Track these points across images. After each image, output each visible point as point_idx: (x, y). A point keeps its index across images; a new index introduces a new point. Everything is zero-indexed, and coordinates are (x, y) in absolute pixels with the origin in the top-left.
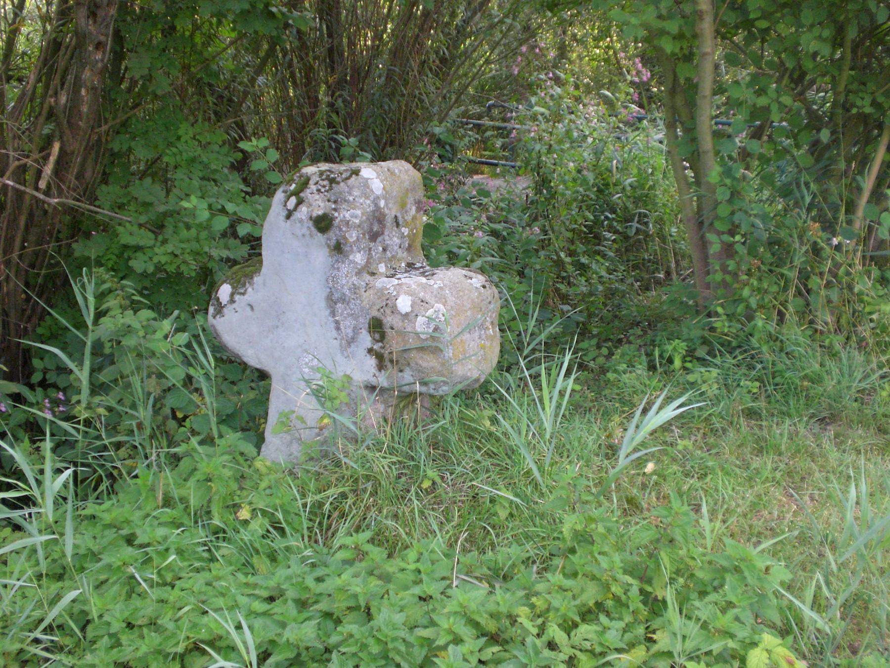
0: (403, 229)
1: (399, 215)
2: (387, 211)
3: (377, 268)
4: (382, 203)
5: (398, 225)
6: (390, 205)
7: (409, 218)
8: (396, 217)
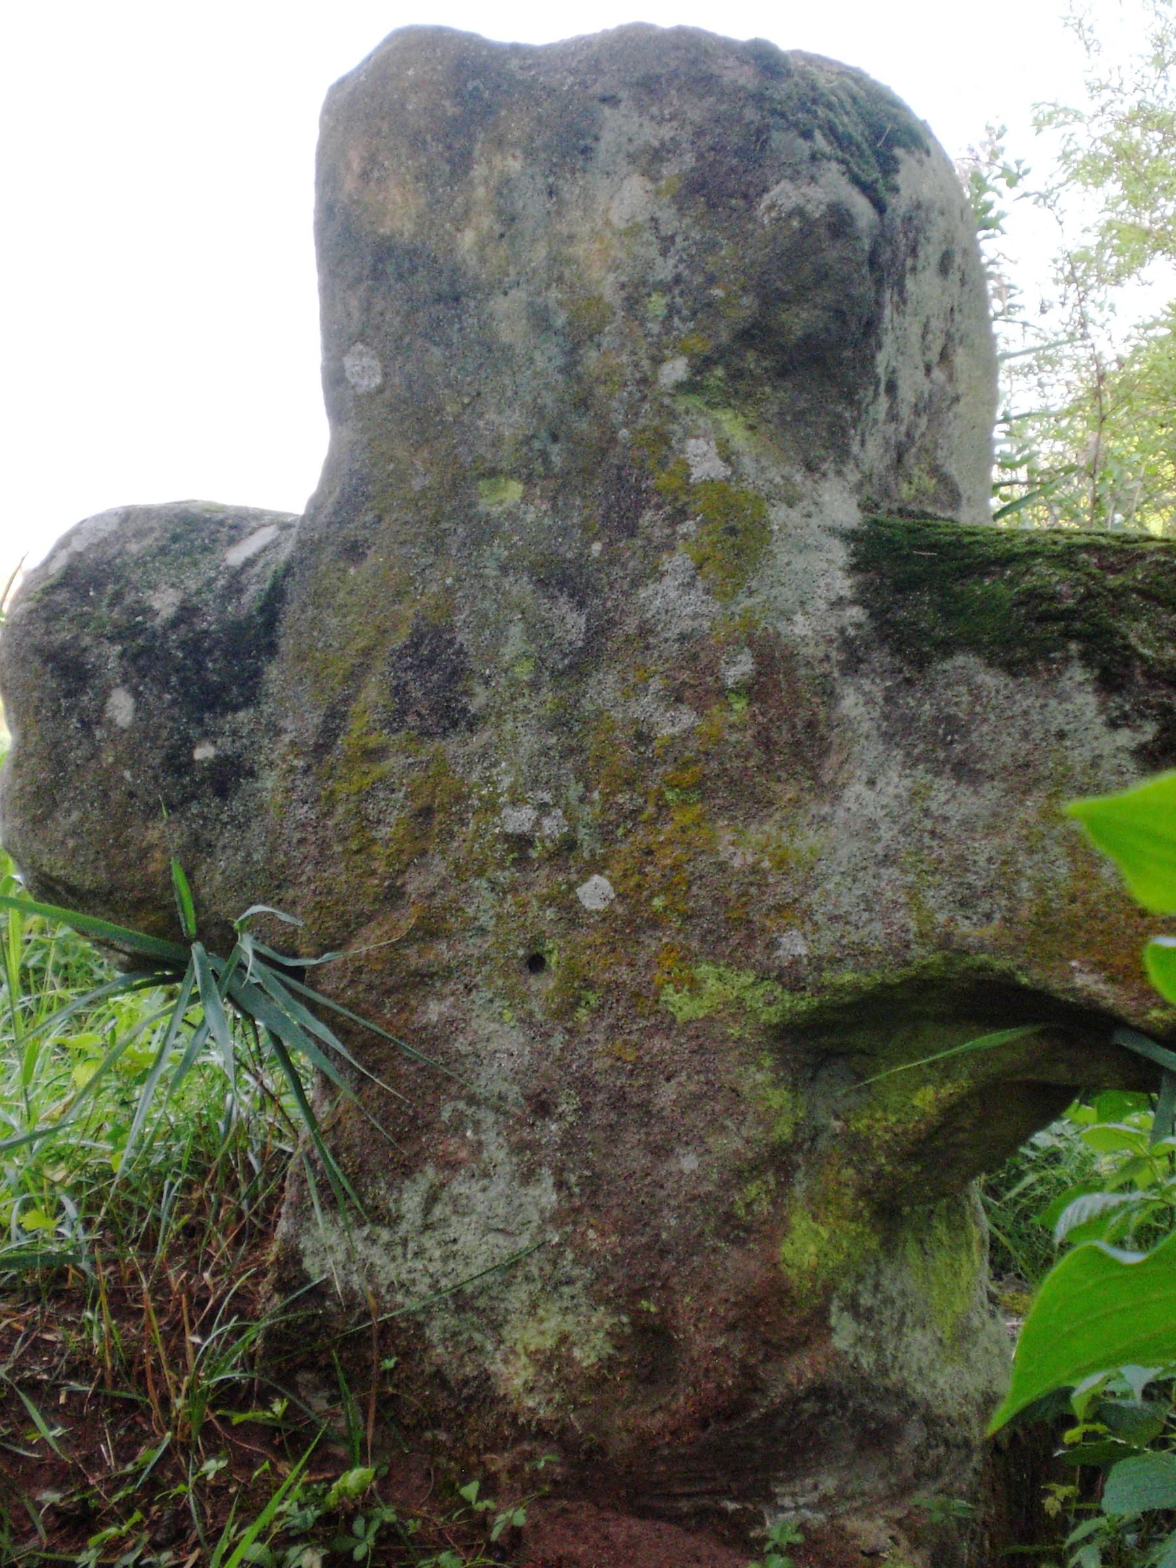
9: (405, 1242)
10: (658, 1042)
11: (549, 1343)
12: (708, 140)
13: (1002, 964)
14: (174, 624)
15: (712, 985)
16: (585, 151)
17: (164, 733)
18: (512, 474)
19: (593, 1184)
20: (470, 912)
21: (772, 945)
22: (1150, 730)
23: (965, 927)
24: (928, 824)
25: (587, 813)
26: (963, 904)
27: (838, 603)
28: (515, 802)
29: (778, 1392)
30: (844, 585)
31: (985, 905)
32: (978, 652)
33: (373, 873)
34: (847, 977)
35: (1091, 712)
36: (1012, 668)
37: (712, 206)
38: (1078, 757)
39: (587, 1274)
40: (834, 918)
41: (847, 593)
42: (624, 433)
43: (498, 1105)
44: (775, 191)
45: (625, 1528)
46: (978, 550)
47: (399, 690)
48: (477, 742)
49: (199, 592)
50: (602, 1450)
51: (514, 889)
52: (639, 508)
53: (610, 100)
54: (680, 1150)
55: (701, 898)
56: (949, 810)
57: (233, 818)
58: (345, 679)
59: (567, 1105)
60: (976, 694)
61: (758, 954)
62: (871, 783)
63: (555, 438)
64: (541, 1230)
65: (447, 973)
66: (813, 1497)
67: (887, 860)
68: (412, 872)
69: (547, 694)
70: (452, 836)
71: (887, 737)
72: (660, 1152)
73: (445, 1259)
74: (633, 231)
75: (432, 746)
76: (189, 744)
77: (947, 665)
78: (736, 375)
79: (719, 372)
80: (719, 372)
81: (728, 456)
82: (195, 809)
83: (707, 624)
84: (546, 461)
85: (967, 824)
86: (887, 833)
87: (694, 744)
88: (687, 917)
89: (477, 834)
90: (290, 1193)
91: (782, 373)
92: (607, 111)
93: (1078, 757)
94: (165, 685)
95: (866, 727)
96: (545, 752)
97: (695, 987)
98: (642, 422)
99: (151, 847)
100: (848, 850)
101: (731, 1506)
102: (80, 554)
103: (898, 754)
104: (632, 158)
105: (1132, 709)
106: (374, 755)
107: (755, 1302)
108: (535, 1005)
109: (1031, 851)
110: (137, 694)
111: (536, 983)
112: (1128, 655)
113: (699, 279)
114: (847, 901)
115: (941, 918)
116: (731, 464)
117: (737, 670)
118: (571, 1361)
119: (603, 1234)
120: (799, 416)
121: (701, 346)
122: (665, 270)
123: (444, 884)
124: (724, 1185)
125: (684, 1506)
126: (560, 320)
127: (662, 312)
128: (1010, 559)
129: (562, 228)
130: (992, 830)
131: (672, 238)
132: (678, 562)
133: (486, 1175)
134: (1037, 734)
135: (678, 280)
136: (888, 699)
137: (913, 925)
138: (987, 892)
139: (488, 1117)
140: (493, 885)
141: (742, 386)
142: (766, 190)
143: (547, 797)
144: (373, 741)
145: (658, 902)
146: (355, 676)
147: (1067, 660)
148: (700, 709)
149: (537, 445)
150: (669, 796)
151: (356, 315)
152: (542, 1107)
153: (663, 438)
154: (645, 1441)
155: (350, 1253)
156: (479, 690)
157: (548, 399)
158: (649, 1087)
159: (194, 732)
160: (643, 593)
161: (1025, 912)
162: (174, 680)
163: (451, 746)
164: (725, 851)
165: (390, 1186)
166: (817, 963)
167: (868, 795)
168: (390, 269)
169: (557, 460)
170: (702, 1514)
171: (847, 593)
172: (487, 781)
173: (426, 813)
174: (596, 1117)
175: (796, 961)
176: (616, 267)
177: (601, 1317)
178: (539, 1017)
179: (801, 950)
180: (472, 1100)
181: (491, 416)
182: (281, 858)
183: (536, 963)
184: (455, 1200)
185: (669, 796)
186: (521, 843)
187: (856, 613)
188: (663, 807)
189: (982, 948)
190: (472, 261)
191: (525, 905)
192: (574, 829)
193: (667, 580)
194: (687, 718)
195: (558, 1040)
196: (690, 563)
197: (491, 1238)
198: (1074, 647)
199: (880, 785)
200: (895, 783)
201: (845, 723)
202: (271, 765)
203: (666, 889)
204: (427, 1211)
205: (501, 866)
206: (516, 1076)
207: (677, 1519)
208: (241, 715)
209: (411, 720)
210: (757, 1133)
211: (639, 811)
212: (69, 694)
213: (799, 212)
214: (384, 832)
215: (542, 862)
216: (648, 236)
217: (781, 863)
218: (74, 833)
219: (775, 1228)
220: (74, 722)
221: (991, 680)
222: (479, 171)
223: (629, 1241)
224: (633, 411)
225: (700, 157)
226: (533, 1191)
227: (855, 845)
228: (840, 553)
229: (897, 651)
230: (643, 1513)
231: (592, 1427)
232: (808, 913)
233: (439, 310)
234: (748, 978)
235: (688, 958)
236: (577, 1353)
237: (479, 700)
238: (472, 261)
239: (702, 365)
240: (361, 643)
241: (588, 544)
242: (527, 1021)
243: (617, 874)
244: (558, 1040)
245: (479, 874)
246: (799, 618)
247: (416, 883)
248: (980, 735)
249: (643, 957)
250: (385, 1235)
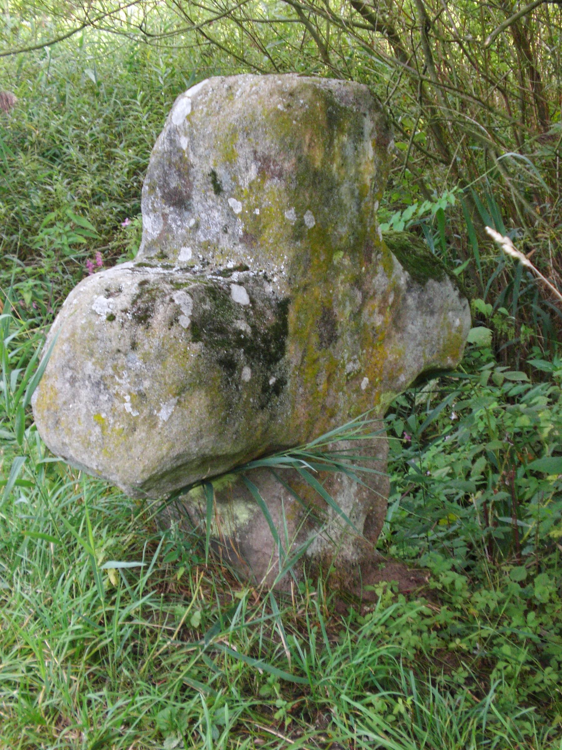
0: (232, 202)
1: (220, 172)
2: (192, 159)
3: (176, 252)
4: (184, 142)
5: (218, 190)
6: (201, 150)
7: (244, 184)
8: (214, 174)
13: (434, 364)
76: (267, 379)
90: (158, 653)
94: (259, 360)
103: (419, 313)
105: (76, 305)
110: (251, 367)
116: (165, 181)
129: (358, 161)
167: (413, 327)
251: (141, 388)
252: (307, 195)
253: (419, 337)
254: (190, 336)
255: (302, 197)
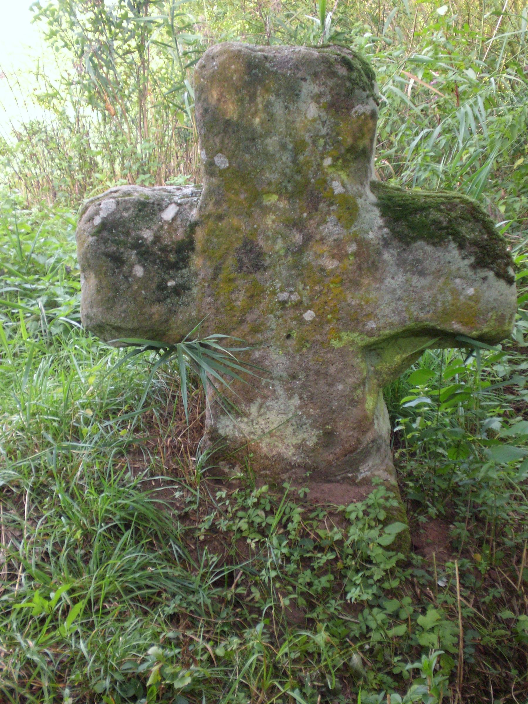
9: (252, 421)
10: (329, 355)
11: (300, 441)
12: (335, 92)
13: (432, 324)
14: (154, 243)
15: (345, 337)
16: (297, 95)
17: (156, 278)
18: (274, 193)
19: (311, 397)
20: (268, 324)
21: (364, 325)
22: (472, 259)
23: (422, 315)
24: (411, 289)
25: (305, 293)
26: (421, 309)
27: (380, 228)
28: (282, 291)
29: (365, 444)
30: (380, 222)
31: (428, 309)
32: (424, 240)
33: (235, 316)
34: (387, 332)
35: (457, 256)
36: (434, 244)
37: (337, 111)
38: (453, 268)
39: (310, 421)
40: (383, 316)
41: (382, 224)
42: (313, 180)
43: (280, 378)
44: (357, 107)
45: (326, 486)
46: (412, 206)
47: (240, 261)
48: (267, 274)
49: (159, 231)
50: (317, 468)
51: (282, 316)
52: (318, 203)
53: (304, 80)
54: (337, 384)
55: (342, 314)
56: (418, 284)
57: (183, 303)
58: (220, 258)
59: (302, 376)
60: (425, 253)
61: (360, 327)
62: (393, 278)
63: (289, 182)
64: (296, 411)
65: (261, 343)
66: (367, 469)
67: (399, 299)
68: (247, 315)
69: (290, 258)
70: (260, 302)
71: (398, 265)
72: (331, 385)
73: (266, 424)
74: (314, 120)
75: (252, 276)
76: (165, 281)
77: (415, 245)
78: (344, 161)
79: (340, 161)
80: (340, 161)
81: (344, 186)
82: (169, 301)
83: (342, 236)
84: (286, 189)
85: (423, 288)
86: (399, 292)
87: (339, 271)
88: (338, 320)
89: (270, 302)
91: (356, 158)
92: (303, 83)
93: (453, 268)
94: (154, 263)
95: (391, 262)
96: (291, 276)
97: (340, 339)
98: (318, 177)
99: (154, 313)
100: (387, 297)
101: (350, 475)
102: (105, 218)
104: (312, 98)
106: (231, 280)
107: (360, 421)
108: (290, 349)
109: (441, 294)
110: (144, 266)
111: (289, 342)
112: (464, 238)
113: (334, 134)
114: (387, 312)
115: (415, 313)
117: (352, 248)
118: (306, 445)
119: (314, 410)
120: (359, 169)
121: (336, 153)
122: (324, 131)
123: (259, 317)
124: (352, 391)
125: (339, 478)
126: (290, 146)
127: (323, 144)
128: (422, 209)
130: (430, 289)
131: (325, 122)
132: (332, 218)
133: (277, 398)
134: (442, 262)
135: (328, 134)
136: (399, 254)
137: (407, 316)
138: (428, 305)
139: (276, 382)
140: (275, 316)
141: (346, 164)
142: (354, 107)
143: (292, 289)
144: (231, 276)
145: (329, 317)
146: (224, 257)
147: (449, 241)
148: (341, 260)
149: (284, 184)
150: (331, 286)
151: (218, 144)
152: (294, 377)
153: (325, 181)
154: (329, 463)
155: (234, 426)
156: (267, 258)
157: (287, 171)
158: (327, 368)
159: (167, 277)
160: (321, 228)
161: (440, 310)
162: (158, 261)
163: (258, 275)
164: (349, 300)
165: (246, 406)
166: (379, 329)
167: (392, 281)
168: (230, 130)
169: (290, 189)
170: (343, 479)
171: (382, 224)
172: (272, 286)
173: (252, 296)
174: (311, 378)
175: (373, 329)
176: (309, 131)
177: (315, 432)
178: (291, 352)
179: (374, 326)
180: (272, 378)
181: (268, 175)
182: (202, 314)
183: (289, 336)
184: (268, 407)
185: (331, 286)
186: (283, 303)
187: (386, 230)
188: (329, 289)
189: (427, 320)
190: (259, 128)
191: (286, 321)
192: (301, 297)
193: (329, 224)
194: (336, 263)
195: (298, 358)
196: (336, 219)
197: (280, 416)
198: (450, 237)
199: (396, 278)
200: (401, 278)
201: (384, 261)
202: (196, 285)
203: (331, 312)
204: (259, 411)
205: (277, 310)
206: (286, 369)
207: (338, 482)
208: (184, 271)
209: (245, 269)
210: (359, 376)
211: (322, 291)
212: (118, 268)
213: (364, 113)
214: (239, 303)
215: (290, 308)
216: (319, 122)
217: (367, 302)
218: (125, 312)
219: (363, 401)
220: (121, 277)
221: (429, 248)
222: (259, 99)
223: (323, 411)
224: (315, 173)
225: (333, 97)
226: (292, 401)
227: (389, 296)
228: (377, 212)
229: (400, 240)
230: (330, 481)
231: (314, 462)
232: (376, 316)
233: (247, 143)
234: (356, 334)
235: (338, 331)
236: (308, 443)
237: (267, 262)
238: (259, 128)
239: (335, 159)
240: (224, 247)
241: (302, 214)
242: (287, 354)
243: (316, 309)
244: (298, 358)
245: (271, 313)
246: (370, 233)
247: (249, 318)
248: (426, 263)
249: (324, 332)
250: (245, 420)
251: (202, 274)
252: (217, 140)
253: (399, 292)
254: (95, 230)
255: (211, 142)
